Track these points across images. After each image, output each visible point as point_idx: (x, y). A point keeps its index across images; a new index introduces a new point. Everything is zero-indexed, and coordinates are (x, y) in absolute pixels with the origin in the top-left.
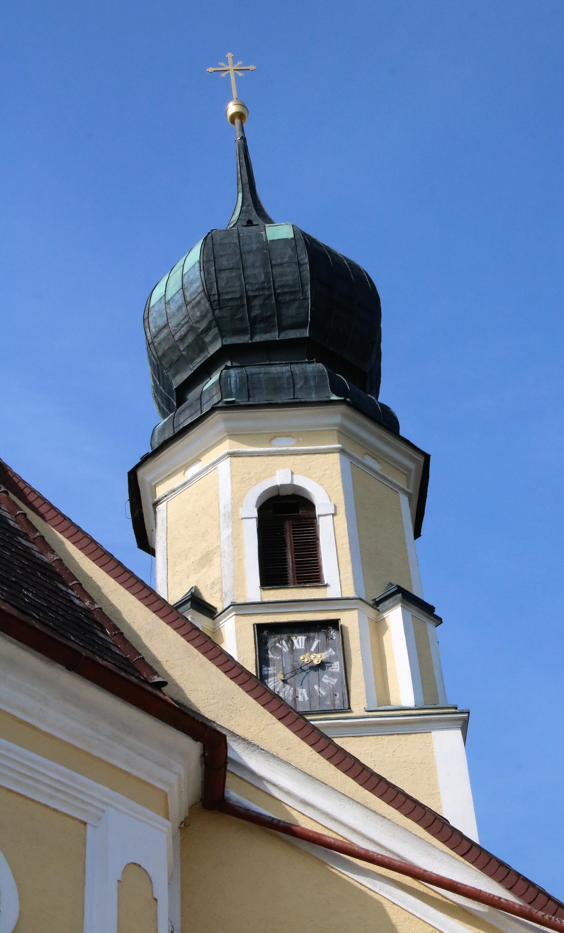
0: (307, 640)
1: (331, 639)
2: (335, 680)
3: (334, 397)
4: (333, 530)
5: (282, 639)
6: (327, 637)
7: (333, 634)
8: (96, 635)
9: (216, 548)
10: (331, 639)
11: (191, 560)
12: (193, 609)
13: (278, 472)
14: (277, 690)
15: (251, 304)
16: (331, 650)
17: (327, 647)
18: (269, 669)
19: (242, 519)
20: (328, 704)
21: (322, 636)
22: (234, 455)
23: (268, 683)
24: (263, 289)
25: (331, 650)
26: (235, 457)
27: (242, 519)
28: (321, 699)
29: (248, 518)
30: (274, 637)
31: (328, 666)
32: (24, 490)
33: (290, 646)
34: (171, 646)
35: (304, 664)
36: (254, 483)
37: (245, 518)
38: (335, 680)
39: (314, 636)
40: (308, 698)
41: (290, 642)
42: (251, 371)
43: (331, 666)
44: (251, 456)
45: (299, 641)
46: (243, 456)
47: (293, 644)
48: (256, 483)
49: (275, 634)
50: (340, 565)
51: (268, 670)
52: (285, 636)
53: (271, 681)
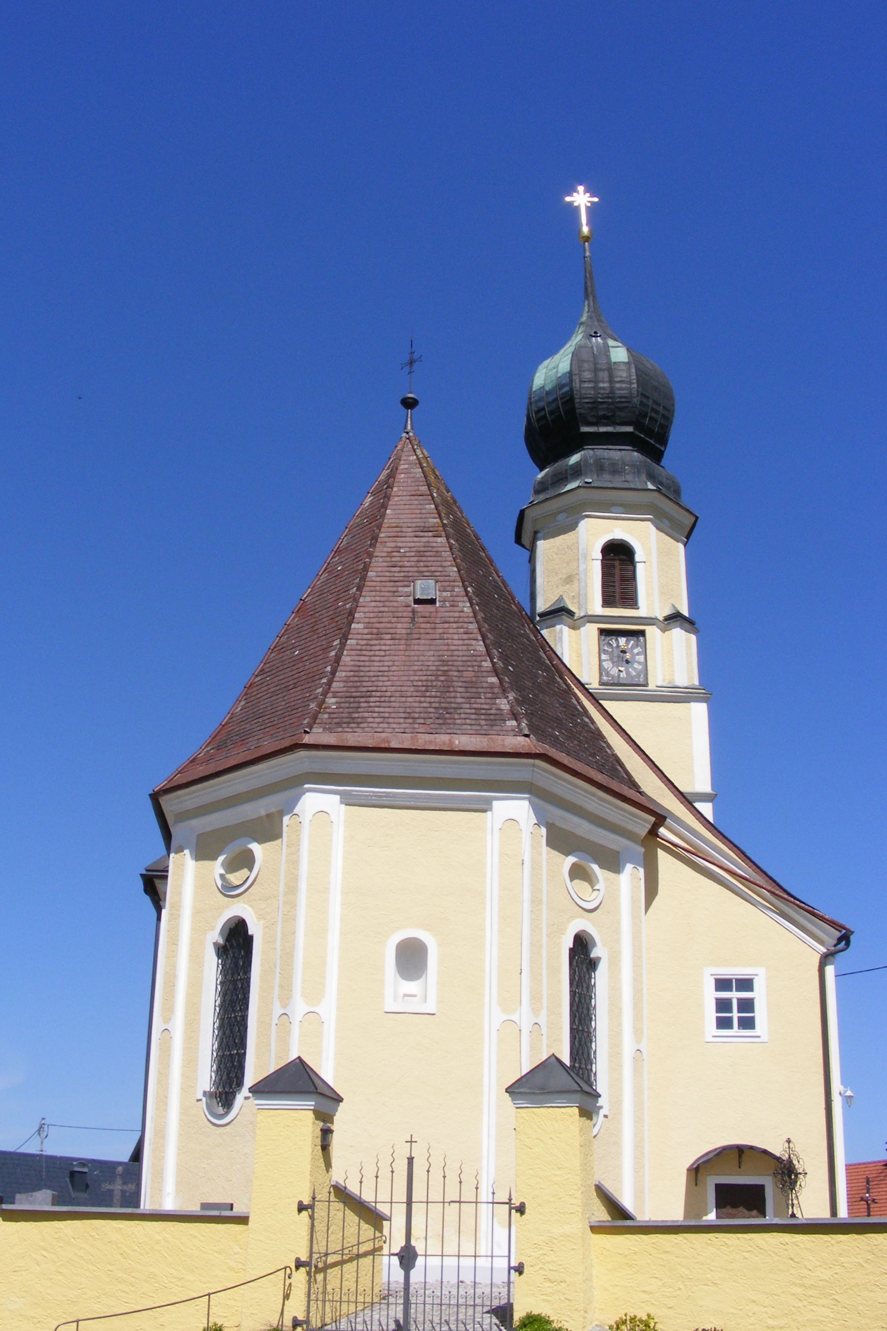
0: (626, 641)
2: (641, 667)
3: (650, 486)
5: (612, 639)
6: (638, 640)
7: (641, 639)
8: (511, 607)
9: (576, 574)
11: (560, 577)
12: (417, 1253)
14: (609, 669)
15: (826, 952)
16: (639, 648)
17: (637, 646)
20: (636, 681)
21: (635, 639)
24: (608, 398)
25: (639, 648)
28: (633, 677)
38: (641, 667)
41: (617, 640)
42: (596, 456)
45: (622, 641)
47: (618, 643)
52: (614, 637)
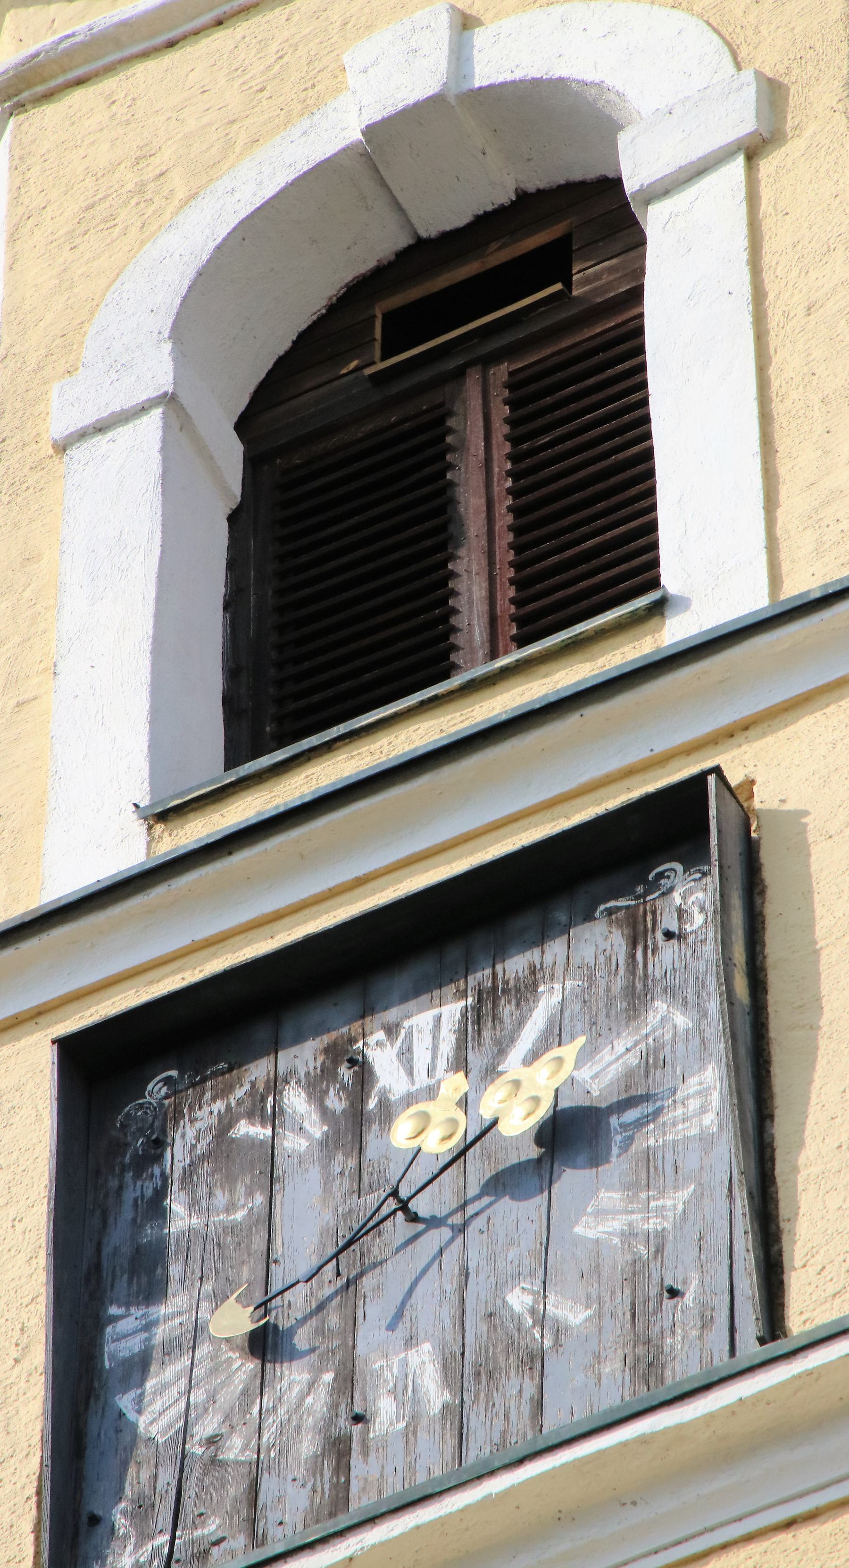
1: (669, 935)
4: (741, 241)
10: (669, 935)
13: (346, 59)
18: (163, 1310)
19: (62, 447)
22: (40, 89)
23: (139, 1412)
26: (48, 96)
27: (62, 447)
29: (100, 428)
30: (223, 1093)
31: (624, 1126)
32: (272, 1057)
33: (336, 1102)
34: (21, 1462)
35: (420, 1174)
36: (181, 194)
37: (83, 435)
39: (533, 972)
40: (448, 1396)
43: (658, 1112)
44: (171, 44)
46: (110, 69)
48: (193, 196)
49: (230, 1070)
50: (783, 443)
51: (149, 1326)
53: (163, 1388)
